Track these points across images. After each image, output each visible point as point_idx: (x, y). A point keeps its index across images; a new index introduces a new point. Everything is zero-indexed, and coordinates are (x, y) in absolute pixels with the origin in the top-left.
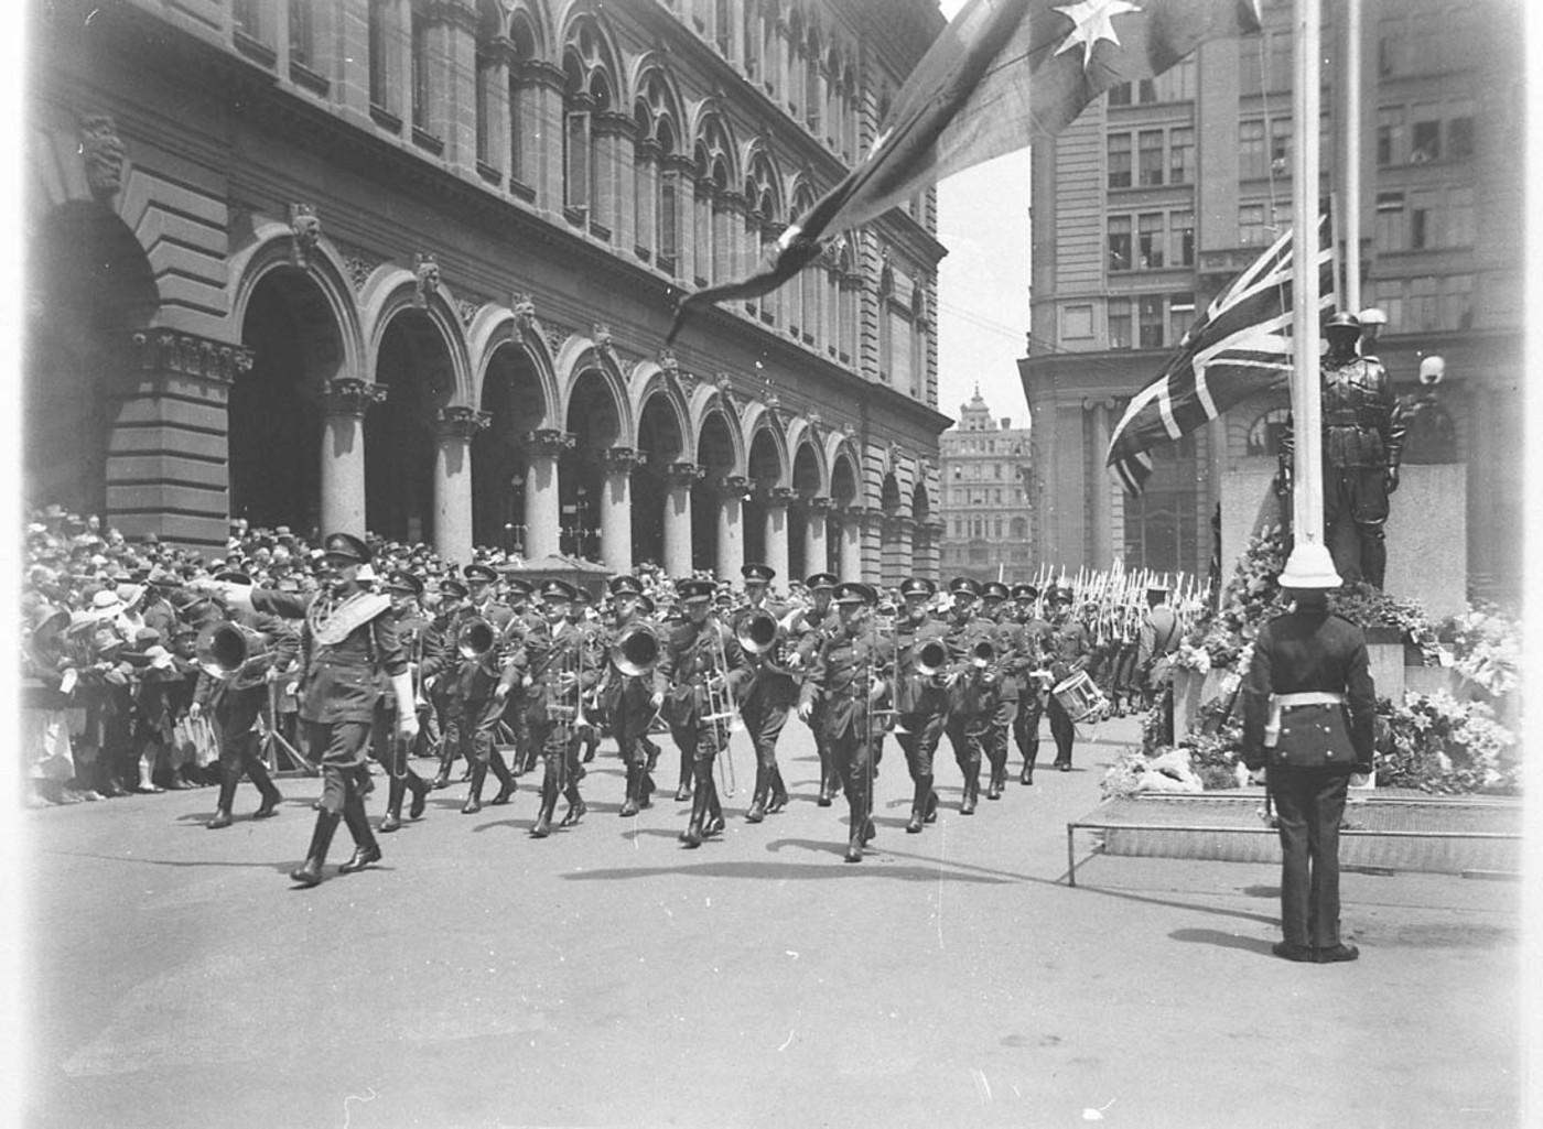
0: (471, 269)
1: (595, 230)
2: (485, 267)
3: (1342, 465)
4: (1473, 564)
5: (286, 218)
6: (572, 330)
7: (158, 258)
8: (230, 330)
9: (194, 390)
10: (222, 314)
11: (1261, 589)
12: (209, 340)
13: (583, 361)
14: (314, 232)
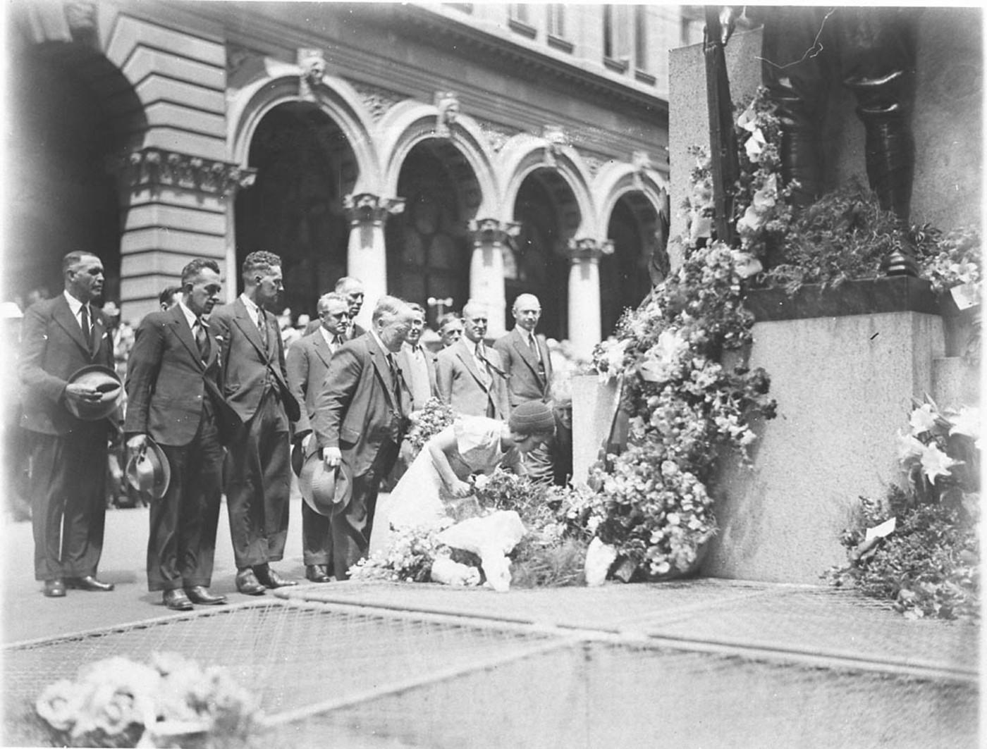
0: (499, 106)
1: (639, 77)
2: (524, 108)
3: (932, 527)
4: (260, 403)
5: (294, 60)
6: (610, 157)
7: (146, 92)
8: (240, 155)
9: (190, 200)
10: (224, 139)
11: (278, 426)
12: (198, 158)
13: (528, 162)
14: (317, 71)
